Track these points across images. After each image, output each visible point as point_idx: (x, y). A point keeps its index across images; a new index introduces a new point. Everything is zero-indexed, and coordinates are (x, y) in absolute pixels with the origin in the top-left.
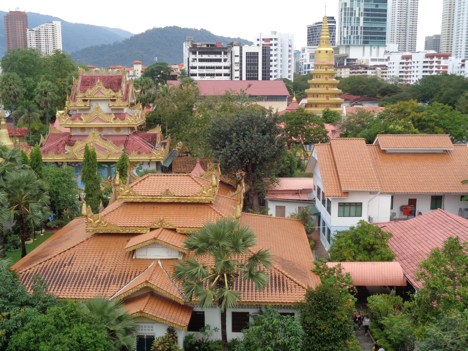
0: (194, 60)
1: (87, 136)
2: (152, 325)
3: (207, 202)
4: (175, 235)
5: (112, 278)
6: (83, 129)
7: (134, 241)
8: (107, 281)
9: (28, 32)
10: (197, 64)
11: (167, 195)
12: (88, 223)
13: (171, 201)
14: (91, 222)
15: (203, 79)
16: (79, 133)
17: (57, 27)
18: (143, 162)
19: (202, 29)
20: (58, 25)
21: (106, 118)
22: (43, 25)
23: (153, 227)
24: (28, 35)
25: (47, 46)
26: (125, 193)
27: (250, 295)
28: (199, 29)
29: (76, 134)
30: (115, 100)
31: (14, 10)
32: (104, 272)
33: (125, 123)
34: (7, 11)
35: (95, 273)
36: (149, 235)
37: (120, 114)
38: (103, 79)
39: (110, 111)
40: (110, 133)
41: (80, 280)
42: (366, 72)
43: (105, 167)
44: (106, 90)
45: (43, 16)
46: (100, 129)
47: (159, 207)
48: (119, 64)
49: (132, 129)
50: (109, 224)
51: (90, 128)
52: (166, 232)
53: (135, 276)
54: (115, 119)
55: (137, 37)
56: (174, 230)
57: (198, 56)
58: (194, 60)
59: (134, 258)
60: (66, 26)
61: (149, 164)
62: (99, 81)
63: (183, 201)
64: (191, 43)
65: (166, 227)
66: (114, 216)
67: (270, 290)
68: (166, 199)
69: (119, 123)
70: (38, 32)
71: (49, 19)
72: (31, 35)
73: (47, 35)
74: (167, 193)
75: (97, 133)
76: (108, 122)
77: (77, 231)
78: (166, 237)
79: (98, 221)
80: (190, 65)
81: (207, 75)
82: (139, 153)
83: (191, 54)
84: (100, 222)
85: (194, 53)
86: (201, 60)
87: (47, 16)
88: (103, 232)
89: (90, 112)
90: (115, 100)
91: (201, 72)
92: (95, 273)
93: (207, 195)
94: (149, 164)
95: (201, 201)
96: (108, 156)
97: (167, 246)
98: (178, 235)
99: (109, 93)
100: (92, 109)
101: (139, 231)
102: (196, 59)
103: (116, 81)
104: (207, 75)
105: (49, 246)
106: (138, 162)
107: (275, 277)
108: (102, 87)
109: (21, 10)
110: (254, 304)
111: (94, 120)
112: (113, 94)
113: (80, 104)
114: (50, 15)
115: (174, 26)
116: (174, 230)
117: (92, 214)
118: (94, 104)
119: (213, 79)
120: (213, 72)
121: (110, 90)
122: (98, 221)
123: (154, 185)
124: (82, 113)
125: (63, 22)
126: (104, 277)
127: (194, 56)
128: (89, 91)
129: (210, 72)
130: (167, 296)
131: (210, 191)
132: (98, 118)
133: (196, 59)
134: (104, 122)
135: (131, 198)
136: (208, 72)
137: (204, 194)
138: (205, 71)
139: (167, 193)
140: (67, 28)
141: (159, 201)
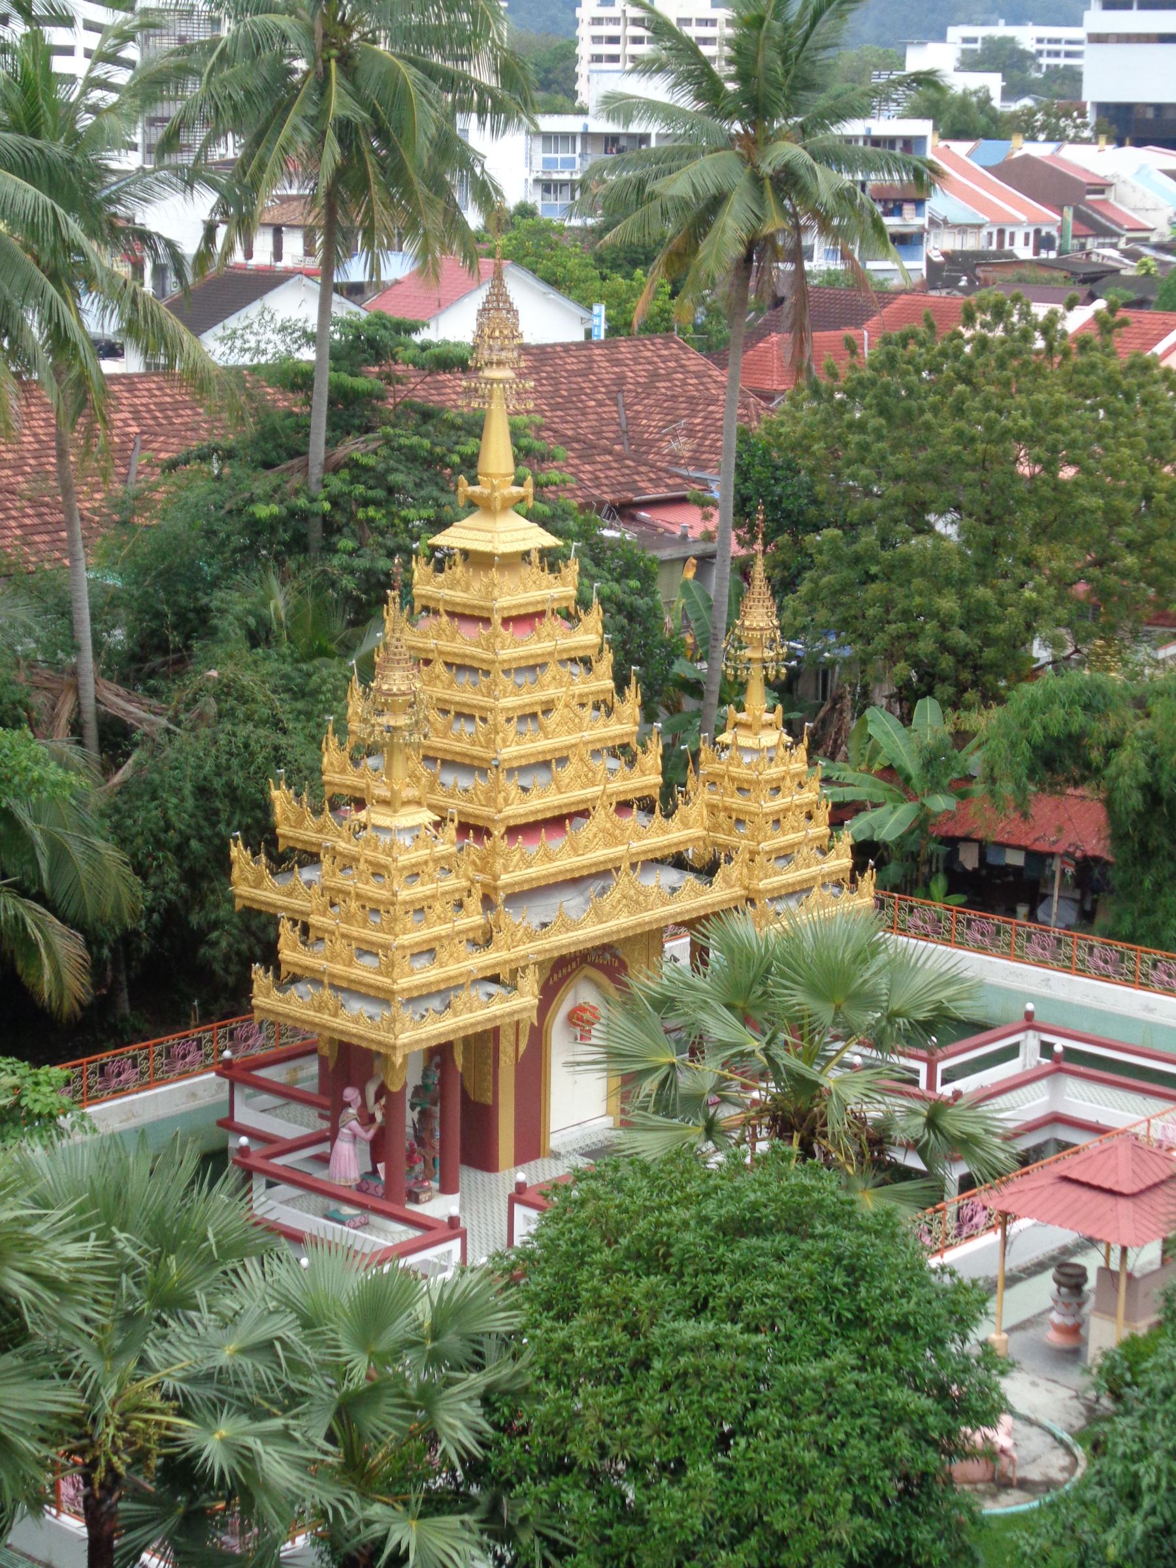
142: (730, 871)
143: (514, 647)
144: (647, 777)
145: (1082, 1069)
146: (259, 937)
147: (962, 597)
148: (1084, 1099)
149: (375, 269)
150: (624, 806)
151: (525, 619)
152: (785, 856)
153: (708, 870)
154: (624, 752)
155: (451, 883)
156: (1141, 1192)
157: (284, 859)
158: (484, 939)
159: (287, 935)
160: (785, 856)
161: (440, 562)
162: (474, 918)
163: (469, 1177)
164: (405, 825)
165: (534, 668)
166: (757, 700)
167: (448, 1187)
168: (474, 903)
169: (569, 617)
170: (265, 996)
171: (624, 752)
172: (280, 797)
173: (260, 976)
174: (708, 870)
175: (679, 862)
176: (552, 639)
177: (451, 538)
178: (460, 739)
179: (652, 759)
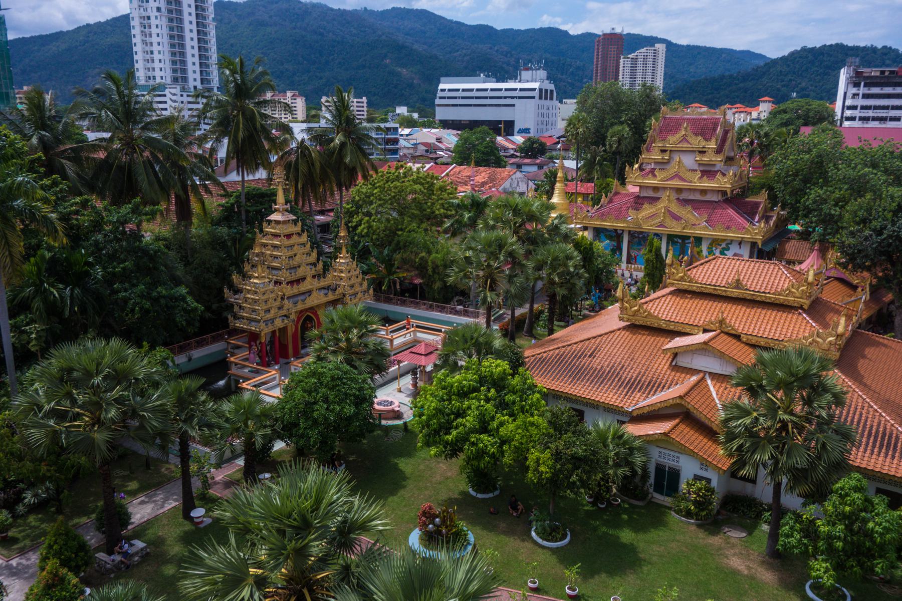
0: (855, 96)
1: (658, 199)
2: (677, 454)
3: (796, 305)
4: (738, 343)
5: (639, 383)
6: (656, 189)
7: (679, 342)
8: (632, 386)
9: (622, 60)
10: (860, 102)
11: (737, 287)
13: (741, 296)
15: (866, 126)
16: (651, 194)
18: (732, 241)
19: (885, 47)
20: (661, 47)
21: (688, 176)
23: (707, 327)
25: (633, 76)
26: (677, 277)
27: (887, 464)
28: (879, 47)
29: (646, 195)
30: (705, 152)
31: (608, 31)
32: (631, 374)
33: (713, 185)
35: (618, 373)
36: (701, 337)
37: (710, 171)
39: (696, 167)
40: (691, 197)
41: (600, 377)
43: (677, 242)
46: (679, 190)
49: (724, 193)
50: (649, 313)
51: (665, 188)
52: (726, 337)
53: (669, 388)
54: (700, 178)
55: (775, 62)
56: (737, 337)
57: (862, 90)
58: (855, 96)
59: (674, 363)
61: (740, 244)
63: (758, 299)
64: (854, 70)
65: (726, 330)
66: (662, 306)
67: (868, 451)
68: (736, 293)
69: (707, 184)
70: (635, 60)
71: (651, 41)
73: (645, 64)
74: (738, 284)
75: (674, 196)
76: (691, 182)
77: (611, 319)
78: (725, 344)
80: (847, 103)
81: (874, 119)
82: (728, 228)
83: (850, 86)
85: (857, 85)
86: (866, 96)
88: (641, 323)
89: (668, 167)
90: (705, 152)
91: (863, 115)
92: (618, 373)
93: (797, 295)
94: (740, 244)
95: (777, 302)
96: (684, 229)
97: (722, 356)
98: (743, 345)
99: (697, 142)
100: (673, 163)
101: (688, 330)
102: (858, 95)
103: (711, 126)
104: (874, 119)
105: (576, 330)
106: (725, 240)
107: (884, 434)
108: (689, 133)
110: (887, 478)
111: (671, 179)
112: (703, 143)
113: (658, 157)
114: (654, 35)
115: (837, 44)
116: (737, 337)
119: (884, 126)
120: (884, 115)
121: (700, 138)
123: (715, 272)
125: (669, 44)
126: (650, 383)
127: (855, 90)
129: (880, 115)
130: (703, 419)
131: (803, 291)
132: (677, 176)
133: (858, 95)
134: (684, 180)
135: (685, 285)
136: (876, 115)
137: (793, 293)
138: (870, 113)
139: (738, 284)
141: (724, 294)
150: (314, 277)
151: (289, 236)
154: (314, 265)
155: (273, 295)
159: (236, 309)
161: (270, 222)
162: (278, 303)
168: (279, 299)
169: (299, 234)
171: (314, 265)
176: (295, 240)
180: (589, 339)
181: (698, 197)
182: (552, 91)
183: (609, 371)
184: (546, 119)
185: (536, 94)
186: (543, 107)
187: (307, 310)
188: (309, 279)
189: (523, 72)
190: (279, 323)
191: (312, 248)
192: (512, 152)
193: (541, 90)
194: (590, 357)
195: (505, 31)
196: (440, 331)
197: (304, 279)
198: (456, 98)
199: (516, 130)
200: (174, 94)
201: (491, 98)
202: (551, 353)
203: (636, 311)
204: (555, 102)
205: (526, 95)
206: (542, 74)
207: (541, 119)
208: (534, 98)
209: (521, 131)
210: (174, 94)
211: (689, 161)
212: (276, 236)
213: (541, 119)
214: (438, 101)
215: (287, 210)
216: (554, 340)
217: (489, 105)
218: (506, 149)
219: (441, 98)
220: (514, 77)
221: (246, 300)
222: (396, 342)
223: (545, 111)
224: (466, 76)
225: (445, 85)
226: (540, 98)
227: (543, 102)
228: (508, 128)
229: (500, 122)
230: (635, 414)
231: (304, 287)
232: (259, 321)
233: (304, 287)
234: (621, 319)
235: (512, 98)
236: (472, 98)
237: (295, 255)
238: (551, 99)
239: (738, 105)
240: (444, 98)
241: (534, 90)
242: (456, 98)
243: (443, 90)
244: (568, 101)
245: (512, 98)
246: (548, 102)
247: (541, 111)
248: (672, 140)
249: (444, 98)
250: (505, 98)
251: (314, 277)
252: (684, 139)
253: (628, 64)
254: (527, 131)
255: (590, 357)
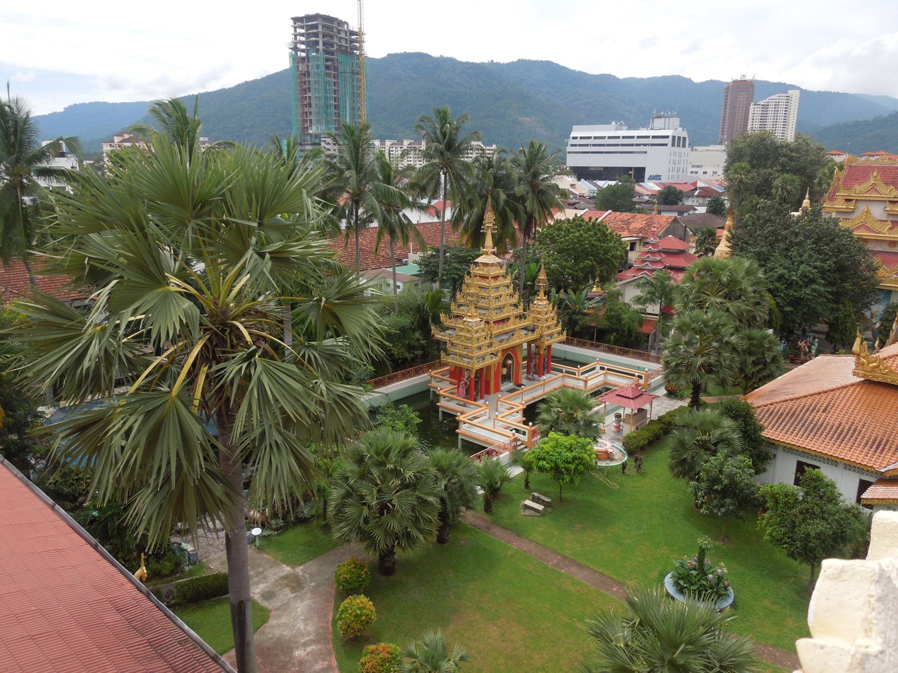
9: (752, 107)
12: (858, 364)
14: (863, 364)
17: (794, 98)
21: (877, 226)
22: (774, 97)
24: (751, 111)
31: (738, 78)
34: (729, 80)
38: (883, 170)
42: (124, 489)
44: (885, 187)
45: (574, 72)
47: (886, 391)
48: (879, 150)
50: (891, 371)
54: (890, 229)
60: (805, 95)
62: (875, 174)
70: (765, 107)
71: (783, 88)
72: (754, 111)
73: (776, 111)
76: (880, 233)
79: (875, 364)
84: (878, 367)
87: (779, 84)
88: (880, 380)
89: (853, 216)
100: (858, 213)
108: (880, 183)
109: (749, 77)
113: (840, 205)
117: (867, 352)
118: (862, 207)
121: (891, 187)
122: (875, 364)
124: (841, 217)
126: (875, 440)
128: (858, 188)
140: (811, 100)
142: (538, 331)
143: (494, 284)
144: (520, 310)
145: (57, 350)
146: (440, 346)
147: (757, 270)
148: (613, 379)
149: (430, 202)
150: (516, 317)
151: (496, 278)
152: (549, 328)
153: (533, 331)
154: (516, 306)
155: (483, 333)
156: (637, 397)
157: (444, 329)
158: (490, 345)
159: (448, 345)
160: (549, 328)
161: (476, 264)
162: (488, 341)
163: (486, 396)
164: (473, 320)
165: (497, 288)
166: (542, 293)
167: (482, 398)
168: (488, 338)
169: (504, 277)
170: (444, 358)
171: (516, 306)
172: (442, 316)
173: (443, 354)
174: (533, 331)
175: (525, 329)
176: (501, 282)
177: (480, 260)
178: (482, 303)
179: (521, 307)
180: (805, 397)
181: (886, 248)
182: (684, 139)
183: (850, 429)
184: (677, 166)
185: (669, 141)
186: (675, 154)
187: (508, 349)
188: (512, 319)
189: (655, 120)
190: (488, 361)
191: (514, 290)
192: (647, 198)
193: (674, 137)
194: (824, 411)
195: (626, 80)
196: (634, 375)
197: (508, 319)
198: (587, 145)
199: (647, 176)
200: (328, 144)
201: (608, 145)
202: (778, 406)
203: (874, 367)
204: (687, 149)
205: (659, 142)
206: (676, 121)
207: (672, 166)
208: (666, 145)
209: (652, 178)
210: (328, 144)
211: (878, 211)
212: (484, 277)
213: (672, 166)
214: (569, 149)
215: (494, 253)
216: (773, 391)
217: (621, 152)
218: (640, 195)
219: (572, 145)
220: (645, 125)
221: (459, 337)
222: (590, 383)
223: (677, 158)
224: (588, 124)
225: (577, 132)
226: (673, 145)
227: (676, 149)
228: (639, 174)
229: (630, 169)
230: (888, 475)
231: (509, 326)
232: (472, 358)
233: (509, 326)
234: (855, 374)
235: (645, 145)
236: (618, 145)
237: (501, 296)
238: (684, 146)
239: (881, 152)
240: (575, 145)
241: (668, 137)
242: (587, 145)
243: (574, 138)
244: (699, 148)
245: (645, 145)
246: (681, 149)
247: (673, 158)
248: (859, 190)
249: (575, 145)
250: (639, 145)
251: (516, 317)
252: (873, 188)
253: (758, 110)
254: (656, 177)
255: (824, 411)
